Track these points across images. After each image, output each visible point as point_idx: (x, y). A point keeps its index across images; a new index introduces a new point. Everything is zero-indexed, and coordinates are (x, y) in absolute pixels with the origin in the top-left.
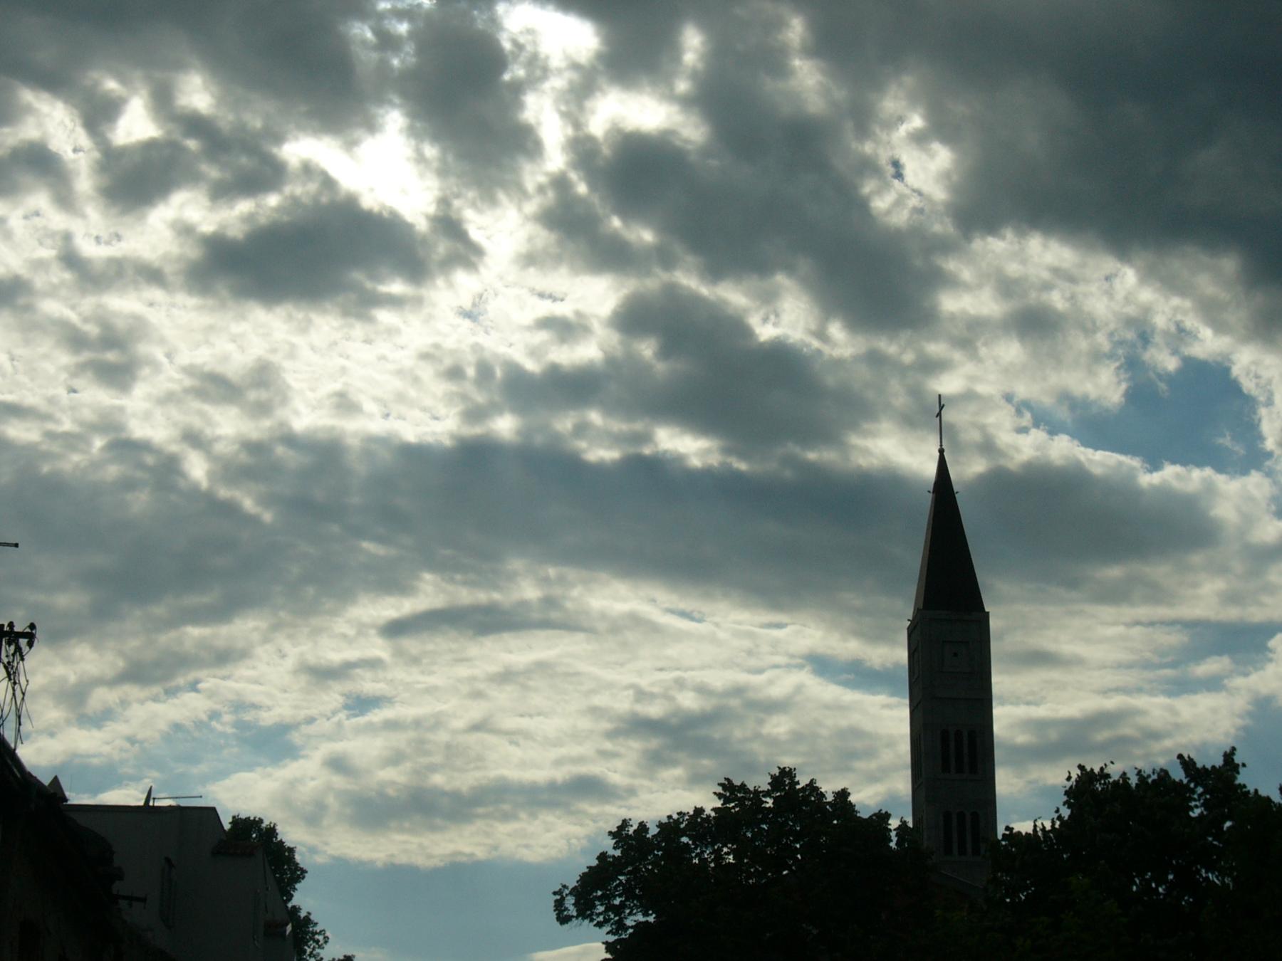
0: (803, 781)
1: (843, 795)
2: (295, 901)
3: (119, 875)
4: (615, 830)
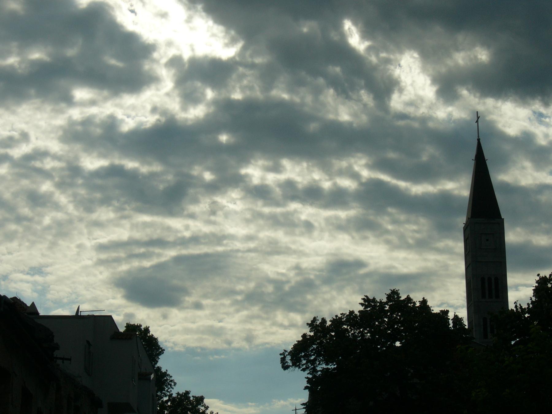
0: (403, 297)
2: (158, 365)
3: (57, 347)
4: (310, 322)
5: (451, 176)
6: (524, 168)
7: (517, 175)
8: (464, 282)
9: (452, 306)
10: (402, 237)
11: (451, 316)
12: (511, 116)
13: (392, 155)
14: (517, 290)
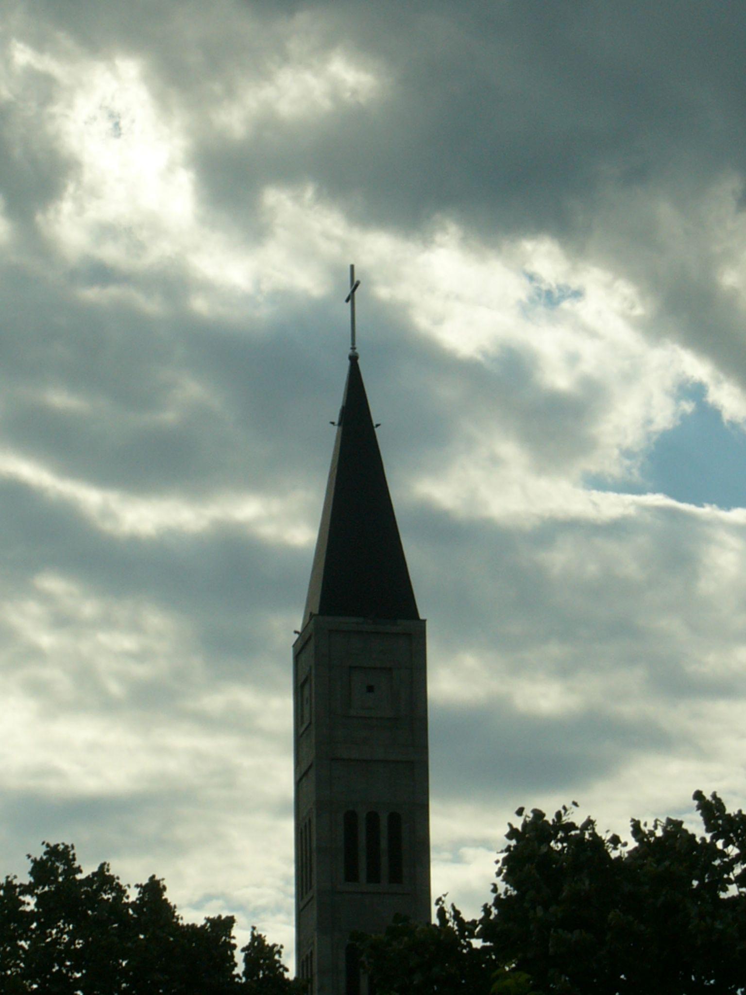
0: (87, 869)
1: (153, 890)
5: (255, 479)
6: (495, 461)
7: (462, 486)
8: (288, 827)
9: (241, 908)
10: (85, 674)
11: (241, 937)
12: (460, 291)
13: (60, 399)
14: (457, 859)
